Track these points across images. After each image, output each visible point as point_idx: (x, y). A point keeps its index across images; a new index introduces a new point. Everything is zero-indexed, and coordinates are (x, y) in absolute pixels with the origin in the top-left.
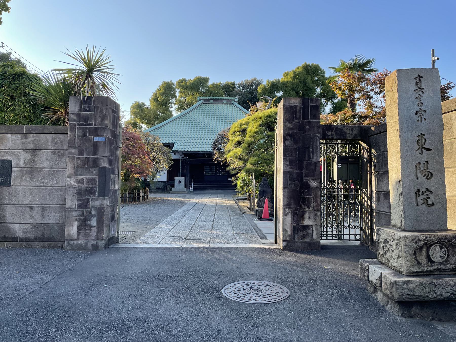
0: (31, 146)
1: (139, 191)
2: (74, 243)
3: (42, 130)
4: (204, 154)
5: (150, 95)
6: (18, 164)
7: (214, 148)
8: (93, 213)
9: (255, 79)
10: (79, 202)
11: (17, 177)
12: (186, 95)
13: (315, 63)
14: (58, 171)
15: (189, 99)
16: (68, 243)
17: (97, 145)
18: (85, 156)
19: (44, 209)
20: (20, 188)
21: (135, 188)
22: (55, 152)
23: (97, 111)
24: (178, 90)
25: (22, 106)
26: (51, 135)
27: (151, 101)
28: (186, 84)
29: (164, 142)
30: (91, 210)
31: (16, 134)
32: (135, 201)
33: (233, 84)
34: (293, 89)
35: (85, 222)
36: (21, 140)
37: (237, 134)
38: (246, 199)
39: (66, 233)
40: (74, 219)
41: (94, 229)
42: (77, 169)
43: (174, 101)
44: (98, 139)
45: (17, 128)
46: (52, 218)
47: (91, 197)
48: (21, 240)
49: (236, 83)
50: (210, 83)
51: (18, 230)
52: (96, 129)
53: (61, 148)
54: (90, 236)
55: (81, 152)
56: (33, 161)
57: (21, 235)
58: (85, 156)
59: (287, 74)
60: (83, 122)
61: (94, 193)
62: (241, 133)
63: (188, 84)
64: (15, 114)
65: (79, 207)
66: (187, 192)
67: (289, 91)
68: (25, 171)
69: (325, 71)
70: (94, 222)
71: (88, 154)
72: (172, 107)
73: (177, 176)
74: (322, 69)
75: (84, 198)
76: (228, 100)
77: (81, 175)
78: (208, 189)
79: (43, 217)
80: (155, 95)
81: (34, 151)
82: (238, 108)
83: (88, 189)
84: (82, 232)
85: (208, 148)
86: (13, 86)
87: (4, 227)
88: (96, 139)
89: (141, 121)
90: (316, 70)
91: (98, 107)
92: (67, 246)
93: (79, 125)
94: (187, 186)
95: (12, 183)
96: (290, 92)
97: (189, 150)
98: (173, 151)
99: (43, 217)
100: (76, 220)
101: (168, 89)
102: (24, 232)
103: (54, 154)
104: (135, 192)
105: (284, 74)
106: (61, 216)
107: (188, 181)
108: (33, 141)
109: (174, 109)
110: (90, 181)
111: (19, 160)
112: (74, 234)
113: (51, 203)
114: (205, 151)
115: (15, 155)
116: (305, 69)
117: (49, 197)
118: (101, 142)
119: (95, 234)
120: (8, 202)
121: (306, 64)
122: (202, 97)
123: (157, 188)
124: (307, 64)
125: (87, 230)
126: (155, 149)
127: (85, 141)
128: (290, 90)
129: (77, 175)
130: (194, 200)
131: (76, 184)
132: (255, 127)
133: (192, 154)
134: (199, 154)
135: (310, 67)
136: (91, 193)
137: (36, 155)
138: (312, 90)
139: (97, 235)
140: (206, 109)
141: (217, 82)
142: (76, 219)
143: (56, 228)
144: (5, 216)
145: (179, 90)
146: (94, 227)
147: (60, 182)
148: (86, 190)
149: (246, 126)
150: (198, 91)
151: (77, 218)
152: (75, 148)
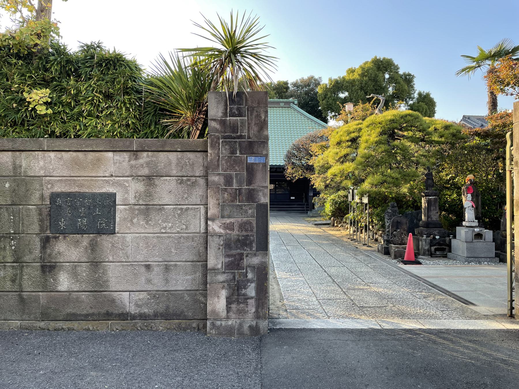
0: (146, 171)
2: (221, 325)
3: (163, 146)
6: (126, 199)
8: (250, 276)
9: (312, 77)
10: (227, 260)
11: (125, 219)
13: (388, 57)
14: (187, 209)
16: (213, 324)
17: (252, 169)
18: (235, 186)
19: (167, 268)
20: (129, 237)
22: (182, 180)
23: (251, 115)
25: (124, 109)
26: (175, 153)
30: (247, 272)
31: (121, 153)
33: (286, 83)
34: (361, 88)
35: (238, 290)
36: (129, 161)
38: (328, 224)
39: (209, 308)
40: (221, 285)
41: (252, 302)
42: (222, 207)
44: (255, 160)
45: (121, 143)
46: (182, 282)
47: (245, 250)
48: (133, 317)
49: (290, 82)
51: (128, 302)
52: (251, 144)
53: (192, 174)
54: (246, 312)
55: (228, 181)
56: (148, 194)
57: (132, 309)
58: (235, 186)
59: (352, 71)
60: (231, 133)
61: (250, 245)
62: (350, 143)
64: (112, 120)
65: (228, 266)
67: (356, 91)
68: (138, 209)
70: (251, 291)
71: (240, 183)
73: (459, 226)
74: (396, 64)
75: (234, 252)
76: (286, 103)
77: (229, 217)
79: (167, 281)
81: (150, 179)
82: (298, 112)
83: (240, 238)
84: (234, 306)
86: (107, 78)
87: (105, 297)
88: (251, 160)
90: (388, 65)
91: (253, 108)
92: (211, 329)
93: (224, 137)
95: (116, 230)
96: (357, 93)
99: (167, 281)
100: (223, 288)
102: (137, 305)
103: (180, 183)
105: (348, 71)
106: (194, 280)
108: (148, 164)
110: (243, 226)
111: (127, 192)
112: (221, 311)
113: (178, 260)
115: (120, 184)
117: (176, 249)
118: (259, 163)
119: (254, 310)
120: (111, 259)
121: (376, 57)
124: (378, 58)
125: (241, 303)
127: (233, 162)
128: (357, 89)
129: (223, 217)
131: (222, 231)
132: (374, 135)
134: (276, 168)
135: (381, 62)
136: (246, 245)
137: (154, 185)
138: (384, 89)
139: (257, 311)
142: (224, 286)
143: (187, 298)
144: (107, 281)
146: (252, 298)
147: (192, 226)
148: (238, 240)
151: (226, 285)
152: (219, 174)
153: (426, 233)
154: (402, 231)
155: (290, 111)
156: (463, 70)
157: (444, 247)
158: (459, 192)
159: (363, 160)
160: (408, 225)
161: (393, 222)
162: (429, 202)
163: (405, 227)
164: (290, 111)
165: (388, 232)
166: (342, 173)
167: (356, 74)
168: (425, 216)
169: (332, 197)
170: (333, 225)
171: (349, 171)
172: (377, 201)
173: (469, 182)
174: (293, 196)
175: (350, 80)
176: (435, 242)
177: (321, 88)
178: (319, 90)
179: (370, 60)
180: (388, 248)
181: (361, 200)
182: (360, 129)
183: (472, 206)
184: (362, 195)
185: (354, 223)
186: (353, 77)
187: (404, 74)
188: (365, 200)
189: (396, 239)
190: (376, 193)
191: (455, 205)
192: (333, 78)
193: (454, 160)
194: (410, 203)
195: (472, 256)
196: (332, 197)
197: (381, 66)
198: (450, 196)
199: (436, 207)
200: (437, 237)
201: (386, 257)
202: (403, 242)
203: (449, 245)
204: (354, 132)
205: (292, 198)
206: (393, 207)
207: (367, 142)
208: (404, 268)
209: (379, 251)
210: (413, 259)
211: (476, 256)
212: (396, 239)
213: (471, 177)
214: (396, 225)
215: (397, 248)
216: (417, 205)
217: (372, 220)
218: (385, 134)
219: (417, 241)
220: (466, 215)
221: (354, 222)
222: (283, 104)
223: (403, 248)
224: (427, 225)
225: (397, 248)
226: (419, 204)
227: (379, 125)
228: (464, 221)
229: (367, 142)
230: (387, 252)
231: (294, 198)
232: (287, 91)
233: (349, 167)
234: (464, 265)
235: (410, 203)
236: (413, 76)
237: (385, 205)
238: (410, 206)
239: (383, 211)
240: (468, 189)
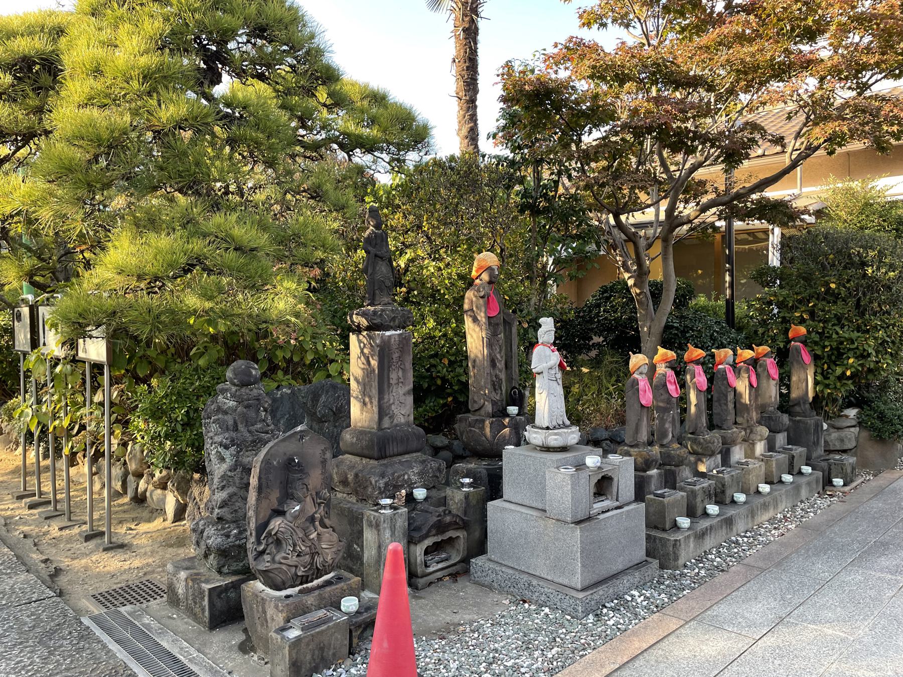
154: (311, 509)
159: (79, 155)
183: (561, 365)
184: (77, 330)
188: (95, 349)
190: (155, 319)
207: (97, 72)
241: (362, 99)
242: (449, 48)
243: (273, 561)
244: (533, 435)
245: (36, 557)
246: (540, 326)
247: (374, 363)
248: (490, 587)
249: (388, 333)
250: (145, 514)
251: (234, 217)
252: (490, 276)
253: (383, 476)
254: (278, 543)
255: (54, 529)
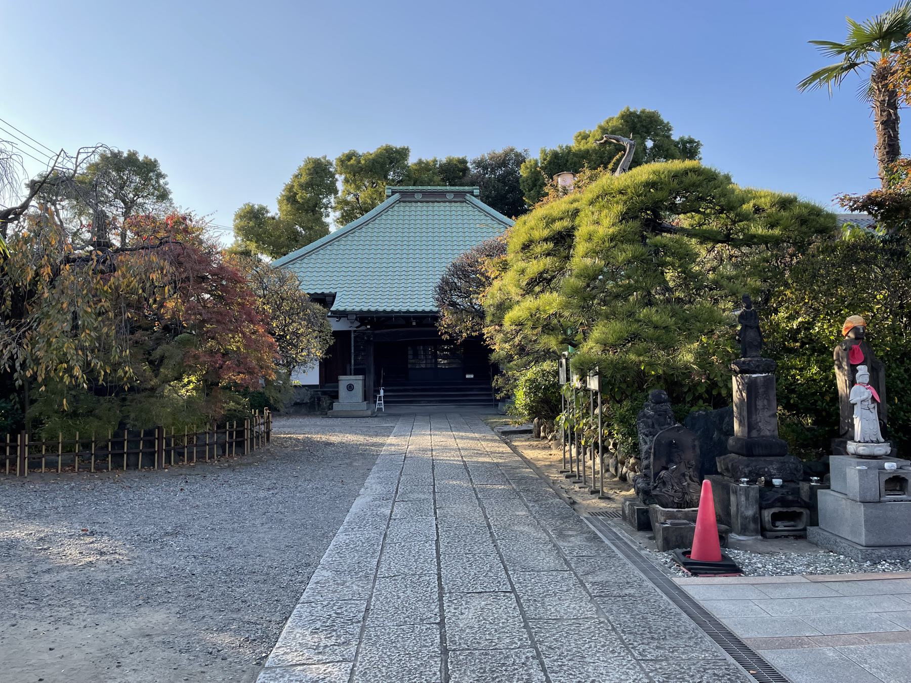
1: (241, 424)
4: (410, 317)
5: (279, 190)
7: (441, 302)
9: (512, 150)
12: (358, 188)
13: (650, 109)
15: (364, 195)
21: (231, 416)
24: (340, 178)
27: (280, 202)
28: (359, 162)
29: (312, 292)
32: (231, 452)
33: (464, 162)
37: (538, 249)
38: (530, 432)
43: (332, 199)
50: (412, 161)
62: (551, 245)
63: (363, 162)
66: (369, 412)
69: (671, 124)
72: (328, 216)
74: (666, 122)
76: (457, 194)
78: (419, 402)
80: (290, 188)
82: (481, 210)
85: (420, 299)
89: (257, 247)
90: (651, 122)
94: (369, 396)
97: (373, 309)
98: (332, 312)
101: (318, 176)
104: (231, 426)
107: (372, 384)
109: (332, 219)
114: (412, 309)
116: (626, 121)
122: (397, 188)
123: (296, 404)
124: (632, 110)
126: (286, 307)
130: (391, 440)
132: (606, 222)
133: (379, 318)
134: (396, 317)
135: (639, 117)
140: (407, 213)
141: (427, 158)
145: (343, 176)
149: (566, 223)
150: (386, 177)
153: (746, 470)
154: (683, 469)
155: (466, 208)
156: (816, 76)
157: (798, 510)
158: (823, 361)
159: (581, 283)
160: (698, 451)
161: (658, 444)
162: (751, 388)
163: (691, 456)
164: (465, 209)
165: (647, 467)
166: (534, 317)
167: (591, 140)
168: (741, 423)
169: (530, 374)
170: (538, 436)
171: (551, 312)
172: (621, 385)
173: (852, 335)
174: (470, 373)
175: (580, 150)
176: (772, 496)
177: (527, 168)
178: (523, 172)
179: (617, 115)
180: (647, 511)
181: (585, 382)
182: (576, 212)
183: (873, 398)
185: (572, 437)
186: (586, 147)
187: (682, 140)
188: (593, 384)
189: (668, 491)
191: (814, 394)
192: (548, 150)
193: (806, 276)
194: (701, 390)
195: (882, 543)
196: (530, 374)
197: (638, 125)
198: (801, 370)
199: (768, 400)
200: (777, 482)
201: (638, 540)
202: (687, 498)
203: (812, 506)
204: (562, 219)
205: (467, 376)
206: (658, 402)
208: (691, 592)
209: (624, 517)
210: (715, 553)
211: (892, 540)
212: (668, 491)
213: (855, 320)
214: (667, 452)
215: (671, 516)
216: (719, 394)
217: (610, 433)
218: (635, 218)
219: (723, 493)
220: (857, 422)
221: (573, 434)
222: (452, 196)
223: (687, 516)
224: (749, 448)
225: (671, 516)
226: (724, 392)
227: (619, 197)
228: (852, 439)
229: (590, 239)
230: (644, 524)
231: (472, 376)
232: (464, 175)
233: (550, 302)
234: (861, 576)
235: (701, 390)
236: (698, 144)
237: (641, 395)
238: (701, 396)
239: (634, 411)
240: (850, 352)
241: (772, 206)
242: (875, 137)
243: (661, 491)
244: (851, 447)
245: (565, 495)
246: (857, 371)
247: (744, 394)
248: (817, 545)
249: (754, 376)
250: (626, 487)
251: (654, 309)
252: (856, 334)
253: (747, 466)
254: (664, 483)
255: (576, 487)
